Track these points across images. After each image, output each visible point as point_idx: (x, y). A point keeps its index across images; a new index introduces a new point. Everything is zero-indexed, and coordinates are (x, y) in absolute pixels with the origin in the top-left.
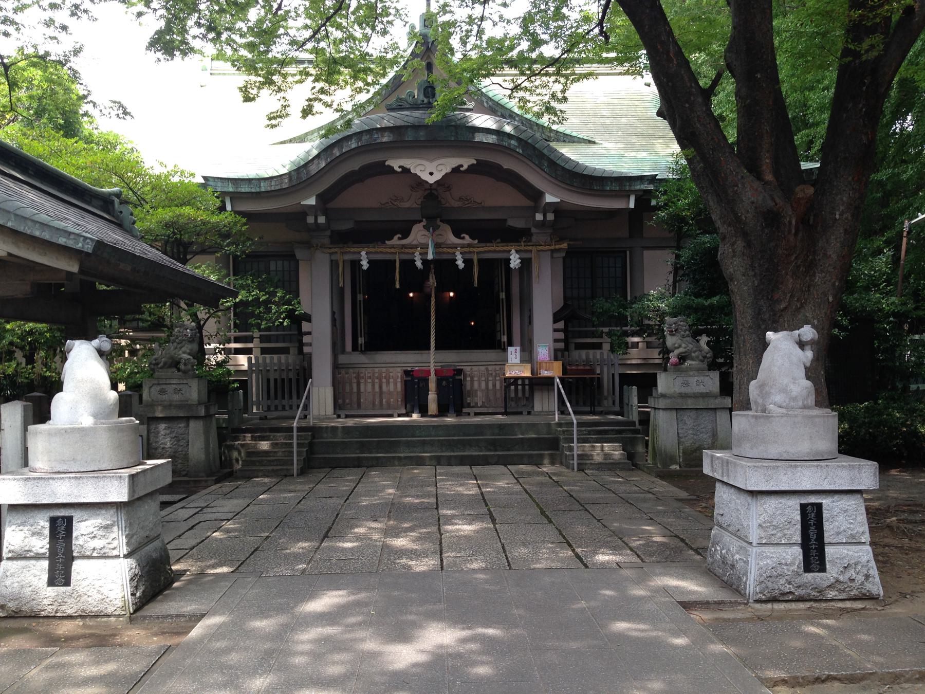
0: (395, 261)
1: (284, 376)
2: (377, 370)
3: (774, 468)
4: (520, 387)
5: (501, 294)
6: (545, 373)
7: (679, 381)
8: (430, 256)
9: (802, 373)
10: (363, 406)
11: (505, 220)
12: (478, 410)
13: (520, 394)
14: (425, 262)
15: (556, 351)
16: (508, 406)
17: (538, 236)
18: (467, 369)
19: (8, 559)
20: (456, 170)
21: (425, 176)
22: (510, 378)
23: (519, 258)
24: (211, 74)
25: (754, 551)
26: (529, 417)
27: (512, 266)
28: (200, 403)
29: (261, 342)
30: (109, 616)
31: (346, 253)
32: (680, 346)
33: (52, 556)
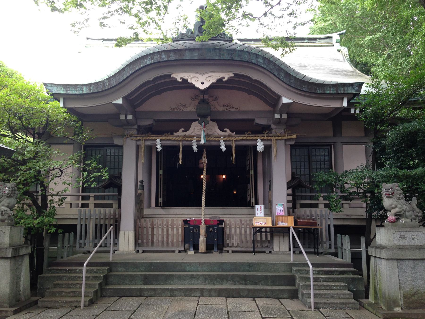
0: (179, 146)
1: (102, 222)
5: (251, 171)
6: (282, 224)
7: (398, 235)
8: (202, 142)
10: (155, 244)
11: (253, 120)
14: (199, 147)
15: (289, 208)
16: (255, 246)
17: (276, 130)
18: (227, 220)
20: (220, 81)
21: (198, 85)
23: (263, 145)
24: (86, 47)
26: (270, 255)
27: (258, 150)
29: (95, 200)
31: (147, 140)
32: (396, 207)
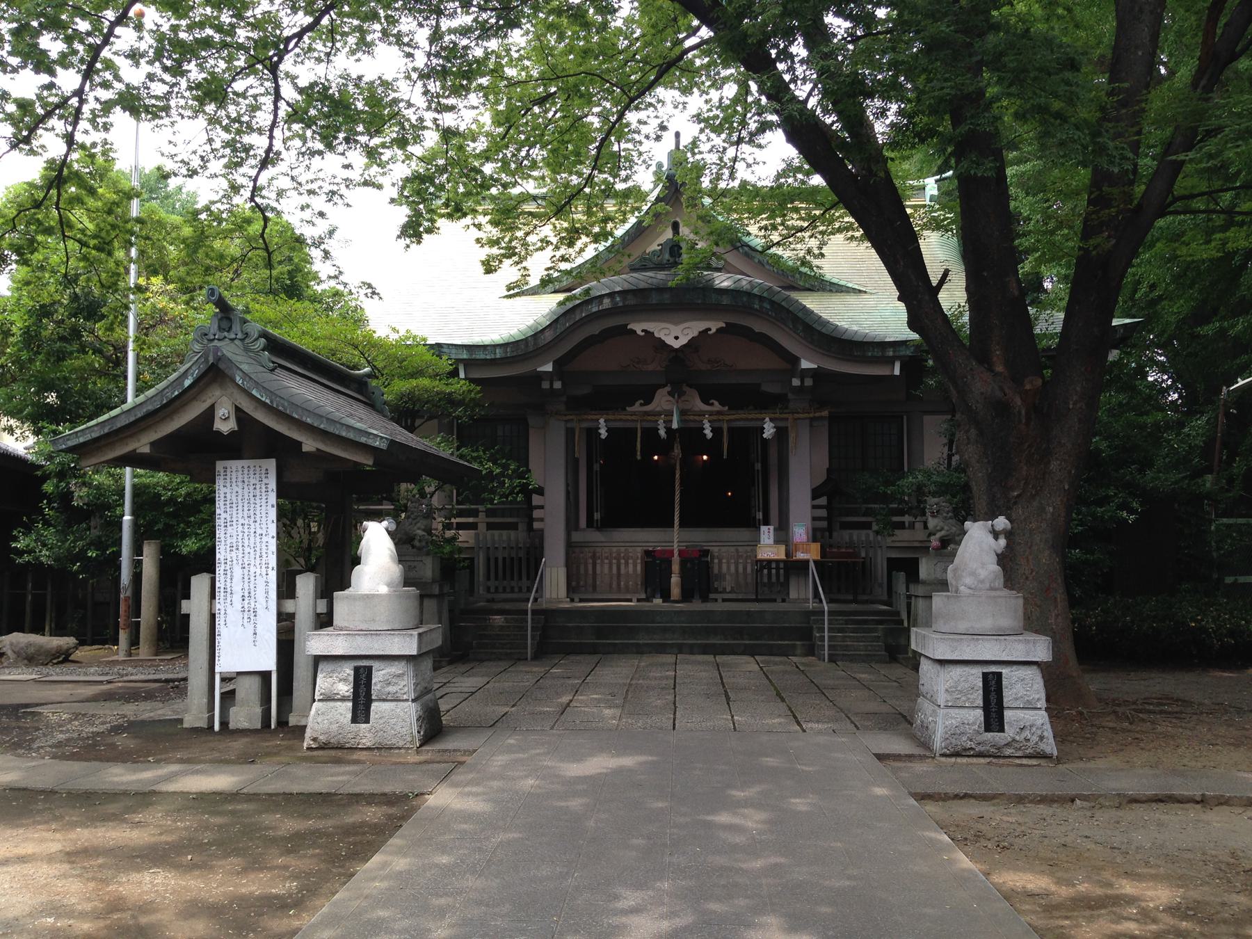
1: (513, 555)
2: (615, 549)
3: (958, 640)
4: (774, 571)
6: (801, 556)
9: (995, 559)
12: (726, 596)
13: (774, 579)
14: (669, 430)
19: (319, 700)
21: (670, 341)
22: (761, 561)
25: (941, 712)
28: (434, 581)
29: (487, 516)
30: (400, 748)
33: (355, 698)
